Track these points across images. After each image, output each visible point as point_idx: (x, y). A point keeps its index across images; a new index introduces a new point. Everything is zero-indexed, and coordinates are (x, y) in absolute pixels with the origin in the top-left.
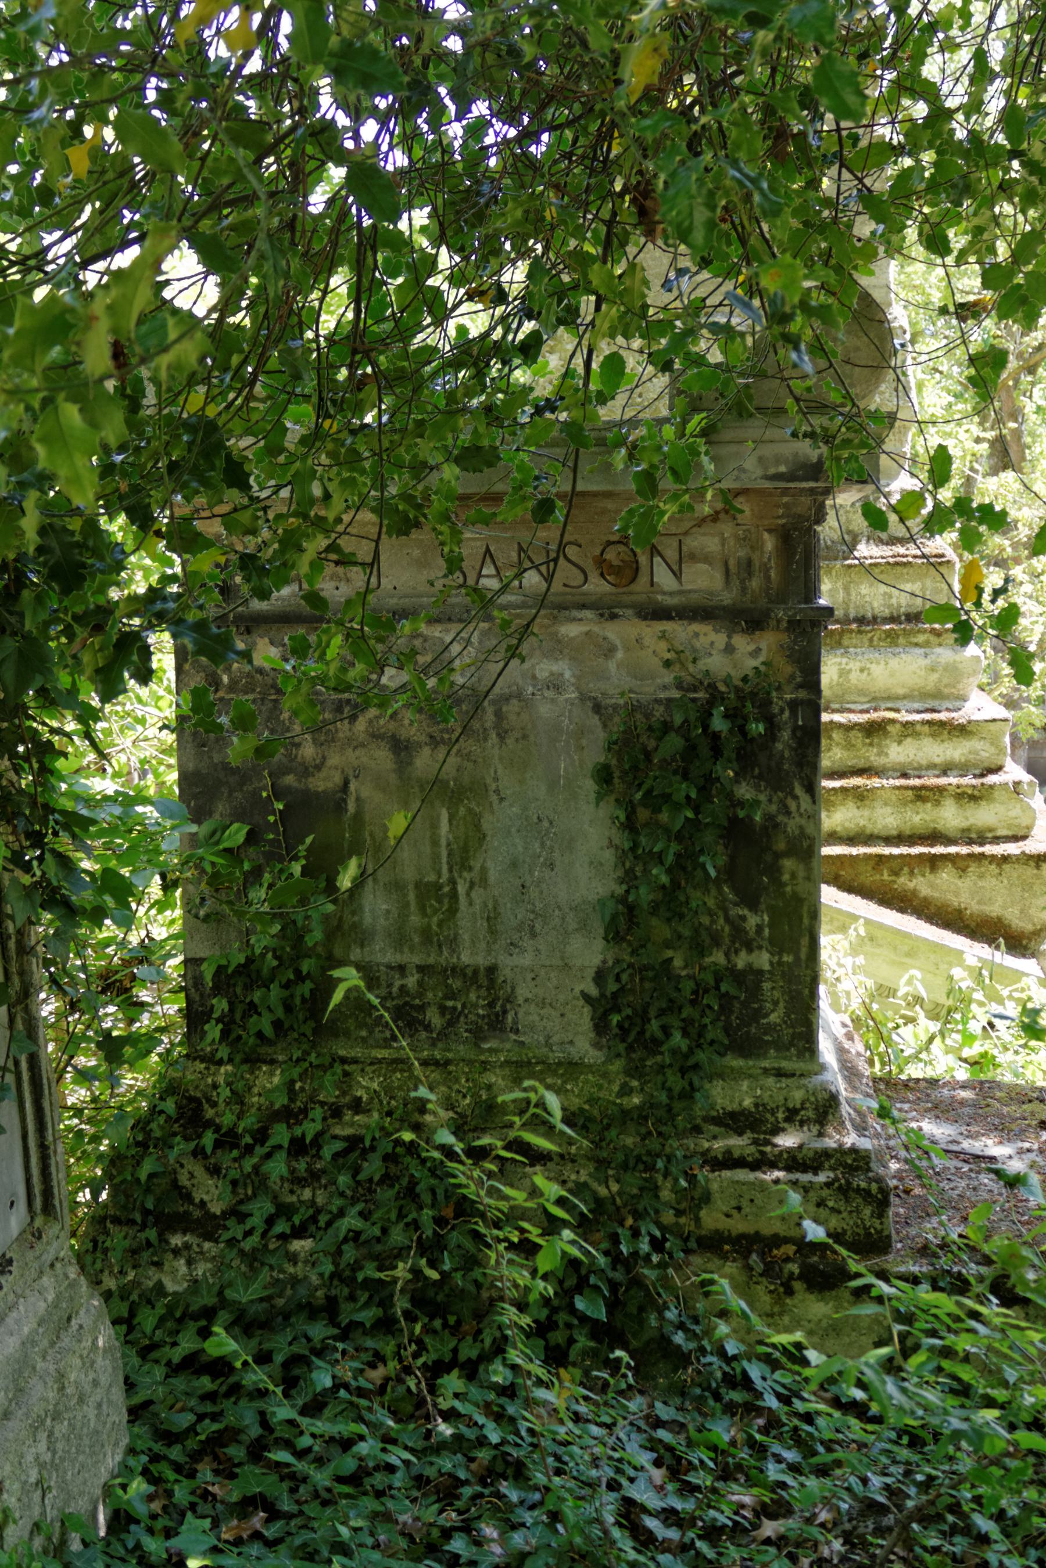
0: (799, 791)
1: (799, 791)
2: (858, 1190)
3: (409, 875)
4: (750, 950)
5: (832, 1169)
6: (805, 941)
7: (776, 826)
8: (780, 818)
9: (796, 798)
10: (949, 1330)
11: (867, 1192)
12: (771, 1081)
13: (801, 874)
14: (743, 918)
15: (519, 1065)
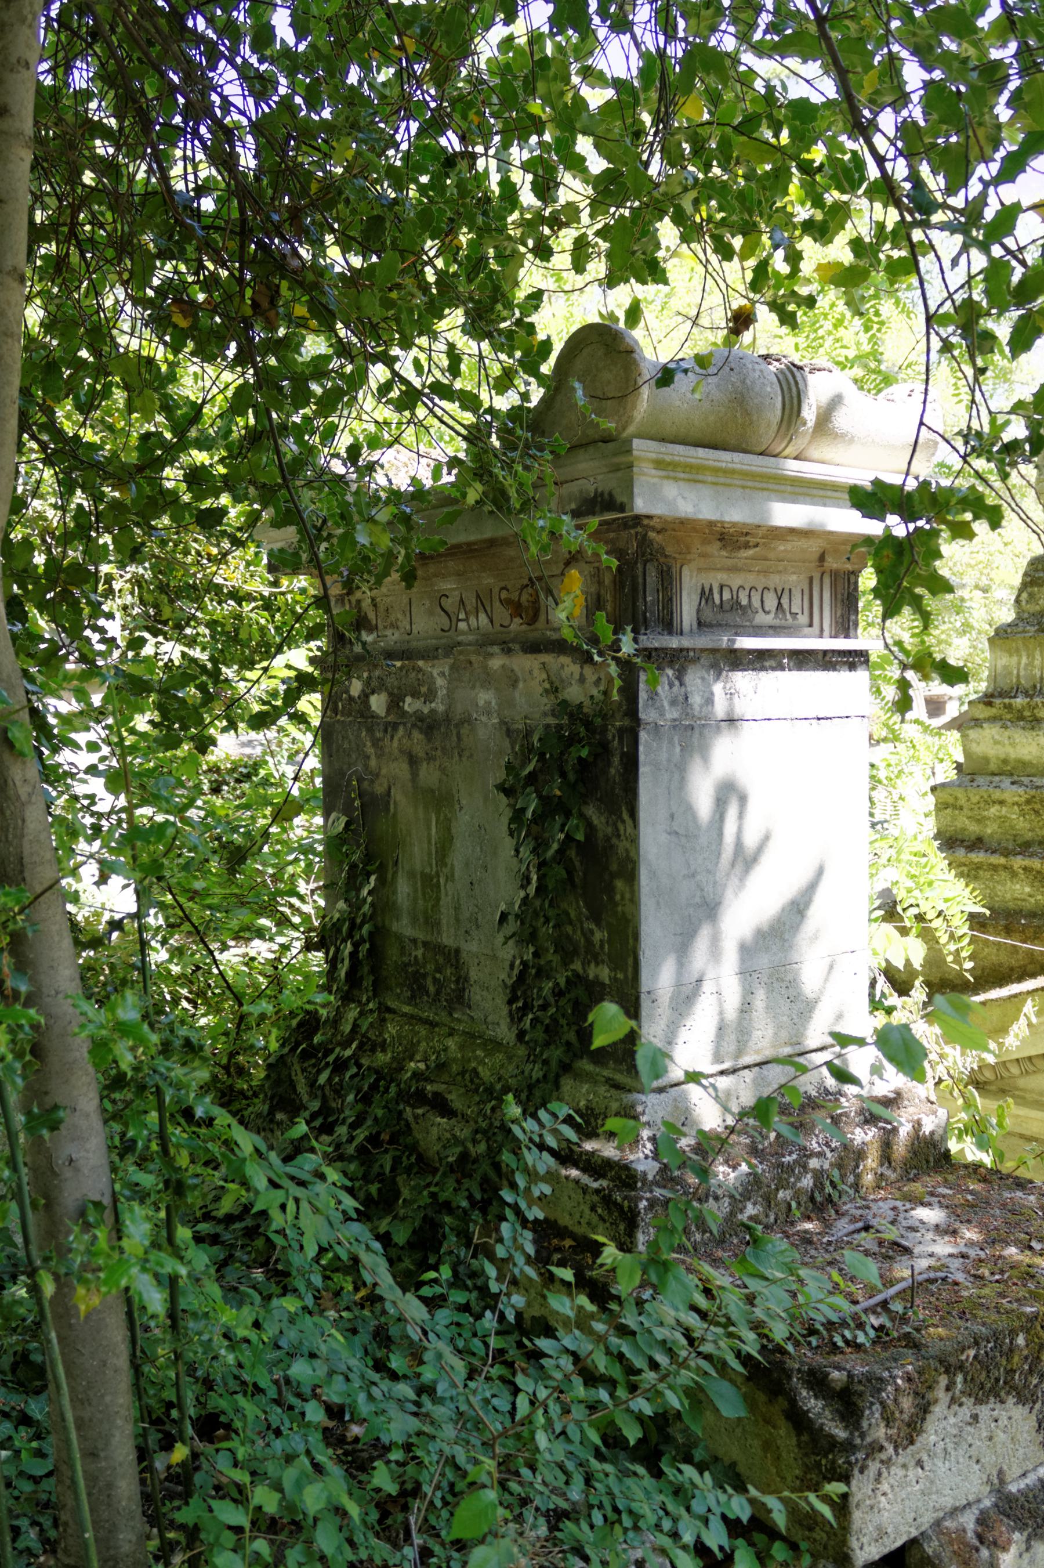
0: (625, 816)
1: (625, 816)
2: (615, 1203)
3: (418, 867)
4: (597, 964)
5: (612, 1180)
6: (630, 961)
7: (612, 846)
8: (614, 841)
9: (623, 822)
10: (722, 1367)
11: (620, 1207)
12: (602, 1090)
13: (628, 896)
14: (592, 932)
15: (471, 1036)
